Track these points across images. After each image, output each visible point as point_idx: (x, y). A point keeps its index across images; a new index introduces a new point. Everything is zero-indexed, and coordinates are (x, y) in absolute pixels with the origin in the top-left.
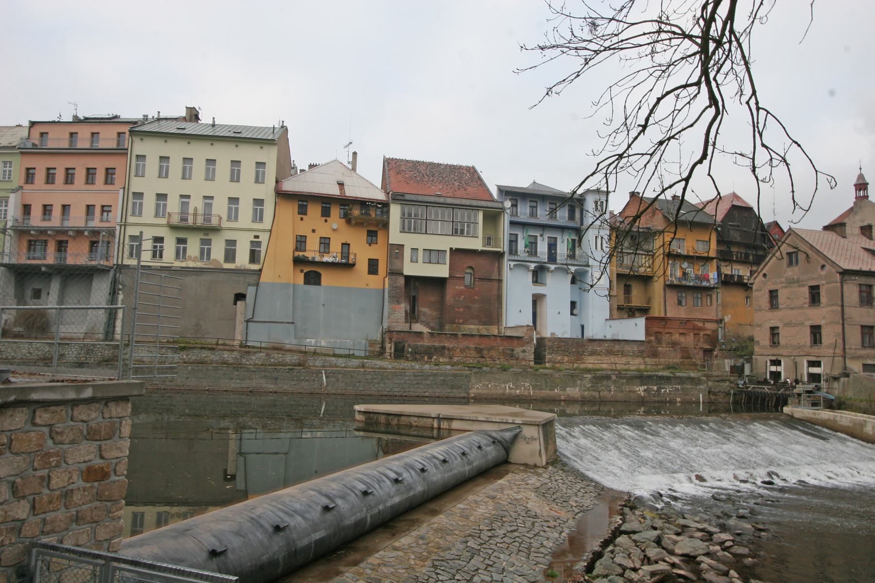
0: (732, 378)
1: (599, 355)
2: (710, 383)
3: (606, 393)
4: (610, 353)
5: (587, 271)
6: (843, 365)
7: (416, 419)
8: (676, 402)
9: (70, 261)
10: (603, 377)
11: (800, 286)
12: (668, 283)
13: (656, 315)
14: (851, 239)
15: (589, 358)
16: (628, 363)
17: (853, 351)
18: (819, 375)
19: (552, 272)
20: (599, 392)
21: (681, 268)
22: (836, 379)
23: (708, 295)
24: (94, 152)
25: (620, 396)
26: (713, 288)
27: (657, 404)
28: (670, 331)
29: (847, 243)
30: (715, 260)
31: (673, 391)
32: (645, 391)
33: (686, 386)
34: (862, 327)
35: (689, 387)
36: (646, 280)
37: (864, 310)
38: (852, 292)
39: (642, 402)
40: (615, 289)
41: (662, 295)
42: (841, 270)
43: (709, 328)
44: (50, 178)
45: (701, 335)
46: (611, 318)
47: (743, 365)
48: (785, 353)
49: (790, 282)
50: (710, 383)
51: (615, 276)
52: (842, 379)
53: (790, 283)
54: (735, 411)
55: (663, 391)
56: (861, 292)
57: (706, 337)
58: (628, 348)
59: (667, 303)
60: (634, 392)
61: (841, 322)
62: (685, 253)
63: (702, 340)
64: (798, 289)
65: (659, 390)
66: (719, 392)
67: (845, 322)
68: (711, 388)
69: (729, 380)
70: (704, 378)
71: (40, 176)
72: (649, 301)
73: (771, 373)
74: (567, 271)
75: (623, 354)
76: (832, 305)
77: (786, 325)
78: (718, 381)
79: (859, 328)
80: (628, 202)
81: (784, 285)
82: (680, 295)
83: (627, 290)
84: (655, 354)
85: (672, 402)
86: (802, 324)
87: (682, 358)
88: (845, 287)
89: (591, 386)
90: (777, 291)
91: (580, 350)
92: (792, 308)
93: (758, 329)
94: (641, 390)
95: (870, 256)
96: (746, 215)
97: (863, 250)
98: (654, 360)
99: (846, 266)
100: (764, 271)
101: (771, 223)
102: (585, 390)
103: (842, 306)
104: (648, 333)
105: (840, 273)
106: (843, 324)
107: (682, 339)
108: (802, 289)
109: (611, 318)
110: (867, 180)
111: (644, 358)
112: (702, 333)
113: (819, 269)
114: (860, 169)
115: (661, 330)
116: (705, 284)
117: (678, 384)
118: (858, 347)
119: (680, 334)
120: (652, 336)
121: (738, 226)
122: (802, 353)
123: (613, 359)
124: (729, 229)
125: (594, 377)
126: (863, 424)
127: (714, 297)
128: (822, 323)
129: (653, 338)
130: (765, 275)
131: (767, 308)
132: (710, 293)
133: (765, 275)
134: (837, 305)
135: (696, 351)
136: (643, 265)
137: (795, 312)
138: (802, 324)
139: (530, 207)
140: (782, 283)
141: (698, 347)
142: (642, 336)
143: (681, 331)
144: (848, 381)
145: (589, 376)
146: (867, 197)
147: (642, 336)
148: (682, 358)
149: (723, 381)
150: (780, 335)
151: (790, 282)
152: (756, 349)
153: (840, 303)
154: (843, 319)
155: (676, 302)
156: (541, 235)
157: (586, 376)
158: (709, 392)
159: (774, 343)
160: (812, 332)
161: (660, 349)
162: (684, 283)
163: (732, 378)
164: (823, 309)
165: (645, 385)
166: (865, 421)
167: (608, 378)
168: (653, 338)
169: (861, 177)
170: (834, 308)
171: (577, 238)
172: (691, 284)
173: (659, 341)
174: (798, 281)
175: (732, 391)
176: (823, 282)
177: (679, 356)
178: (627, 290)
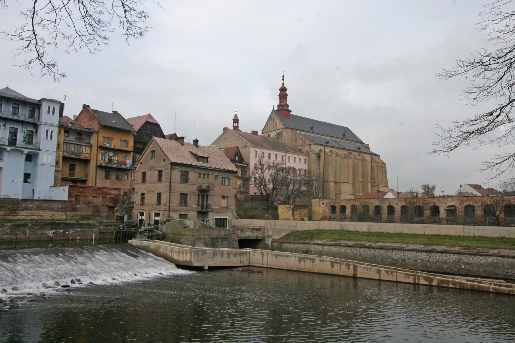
0: (117, 224)
1: (31, 210)
2: (101, 227)
3: (22, 236)
4: (39, 208)
5: (38, 154)
6: (168, 215)
8: (77, 239)
10: (21, 225)
12: (99, 165)
13: (90, 185)
14: (186, 147)
15: (22, 212)
16: (54, 215)
17: (174, 207)
18: (158, 221)
19: (8, 152)
20: (16, 235)
21: (109, 156)
22: (165, 223)
23: (126, 174)
25: (33, 237)
26: (129, 170)
27: (62, 242)
28: (86, 194)
29: (182, 148)
30: (132, 153)
31: (75, 233)
32: (54, 233)
33: (84, 229)
34: (181, 194)
35: (86, 230)
36: (86, 162)
37: (182, 185)
38: (177, 174)
39: (50, 240)
40: (61, 166)
41: (94, 172)
42: (171, 163)
43: (113, 193)
45: (108, 198)
46: (55, 185)
47: (124, 215)
48: (146, 209)
50: (101, 227)
51: (61, 158)
52: (167, 223)
54: (116, 242)
55: (67, 233)
56: (182, 175)
57: (111, 199)
58: (54, 205)
59: (98, 177)
60: (45, 234)
61: (169, 191)
62: (113, 147)
63: (107, 200)
65: (64, 232)
66: (106, 232)
67: (171, 191)
68: (101, 230)
69: (114, 225)
70: (98, 224)
72: (87, 175)
73: (140, 220)
74: (22, 152)
75: (50, 209)
78: (107, 226)
79: (179, 194)
80: (82, 111)
81: (148, 169)
82: (118, 173)
83: (72, 168)
84: (74, 209)
85: (74, 240)
87: (93, 212)
88: (173, 172)
89: (10, 231)
90: (145, 172)
91: (15, 206)
94: (50, 233)
95: (192, 156)
96: (155, 128)
97: (189, 152)
98: (73, 213)
99: (174, 160)
100: (141, 161)
101: (172, 134)
102: (4, 234)
103: (170, 182)
104: (70, 196)
105: (170, 164)
106: (170, 193)
107: (95, 200)
109: (55, 185)
110: (239, 118)
111: (65, 212)
112: (108, 197)
113: (163, 161)
114: (236, 111)
115: (80, 194)
116: (123, 167)
117: (79, 228)
118: (178, 205)
119: (93, 197)
120: (73, 198)
121: (149, 134)
123: (41, 212)
124: (143, 135)
125: (13, 225)
126: (159, 248)
127: (130, 175)
128: (162, 191)
129: (73, 199)
131: (141, 182)
132: (127, 172)
133: (141, 163)
134: (168, 182)
135: (103, 208)
136: (85, 152)
139: (13, 107)
141: (104, 205)
142: (66, 198)
143: (94, 195)
144: (169, 224)
145: (9, 224)
146: (238, 127)
147: (66, 198)
148: (93, 212)
149: (111, 225)
153: (169, 181)
154: (170, 190)
155: (104, 177)
156: (4, 125)
157: (6, 224)
158: (100, 233)
159: (143, 203)
161: (78, 206)
162: (109, 165)
163: (117, 224)
164: (163, 184)
165: (54, 229)
166: (160, 245)
167: (25, 225)
168: (73, 199)
169: (236, 116)
171: (35, 130)
172: (115, 166)
173: (78, 201)
175: (115, 232)
177: (91, 210)
178: (72, 168)
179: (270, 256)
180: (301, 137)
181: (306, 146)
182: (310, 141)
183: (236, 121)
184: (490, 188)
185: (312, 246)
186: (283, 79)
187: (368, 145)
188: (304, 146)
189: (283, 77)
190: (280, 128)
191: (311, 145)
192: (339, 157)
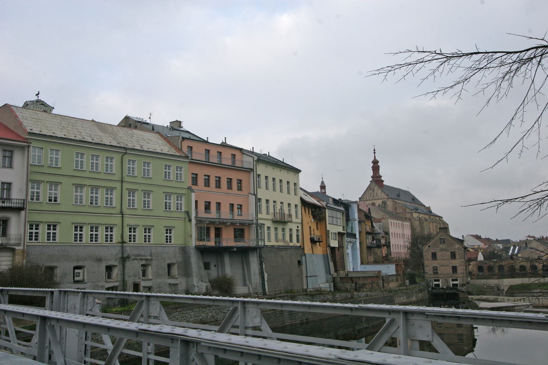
7: (505, 308)
9: (224, 244)
11: (447, 251)
18: (457, 284)
24: (219, 166)
44: (207, 183)
48: (441, 277)
49: (442, 250)
53: (442, 250)
64: (446, 252)
71: (201, 181)
76: (460, 259)
77: (440, 266)
86: (448, 266)
92: (443, 260)
93: (427, 267)
104: (397, 271)
108: (448, 252)
122: (449, 276)
128: (457, 265)
130: (429, 246)
133: (429, 246)
134: (463, 259)
137: (445, 261)
138: (448, 266)
140: (438, 250)
142: (394, 272)
146: (325, 193)
147: (394, 272)
150: (438, 270)
151: (442, 250)
152: (426, 275)
160: (452, 269)
164: (458, 261)
169: (323, 182)
170: (462, 260)
174: (446, 250)
176: (457, 251)
179: (543, 299)
180: (401, 206)
181: (407, 214)
182: (411, 210)
183: (323, 187)
184: (487, 237)
185: (536, 294)
186: (375, 153)
187: (429, 207)
188: (405, 214)
189: (374, 150)
190: (382, 197)
191: (412, 213)
192: (428, 222)
